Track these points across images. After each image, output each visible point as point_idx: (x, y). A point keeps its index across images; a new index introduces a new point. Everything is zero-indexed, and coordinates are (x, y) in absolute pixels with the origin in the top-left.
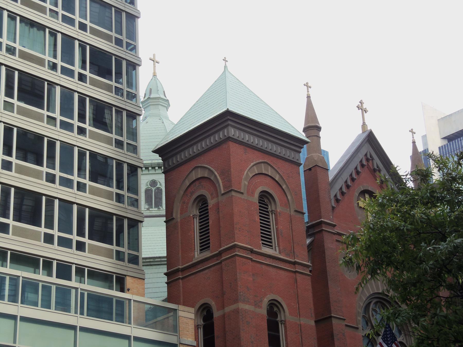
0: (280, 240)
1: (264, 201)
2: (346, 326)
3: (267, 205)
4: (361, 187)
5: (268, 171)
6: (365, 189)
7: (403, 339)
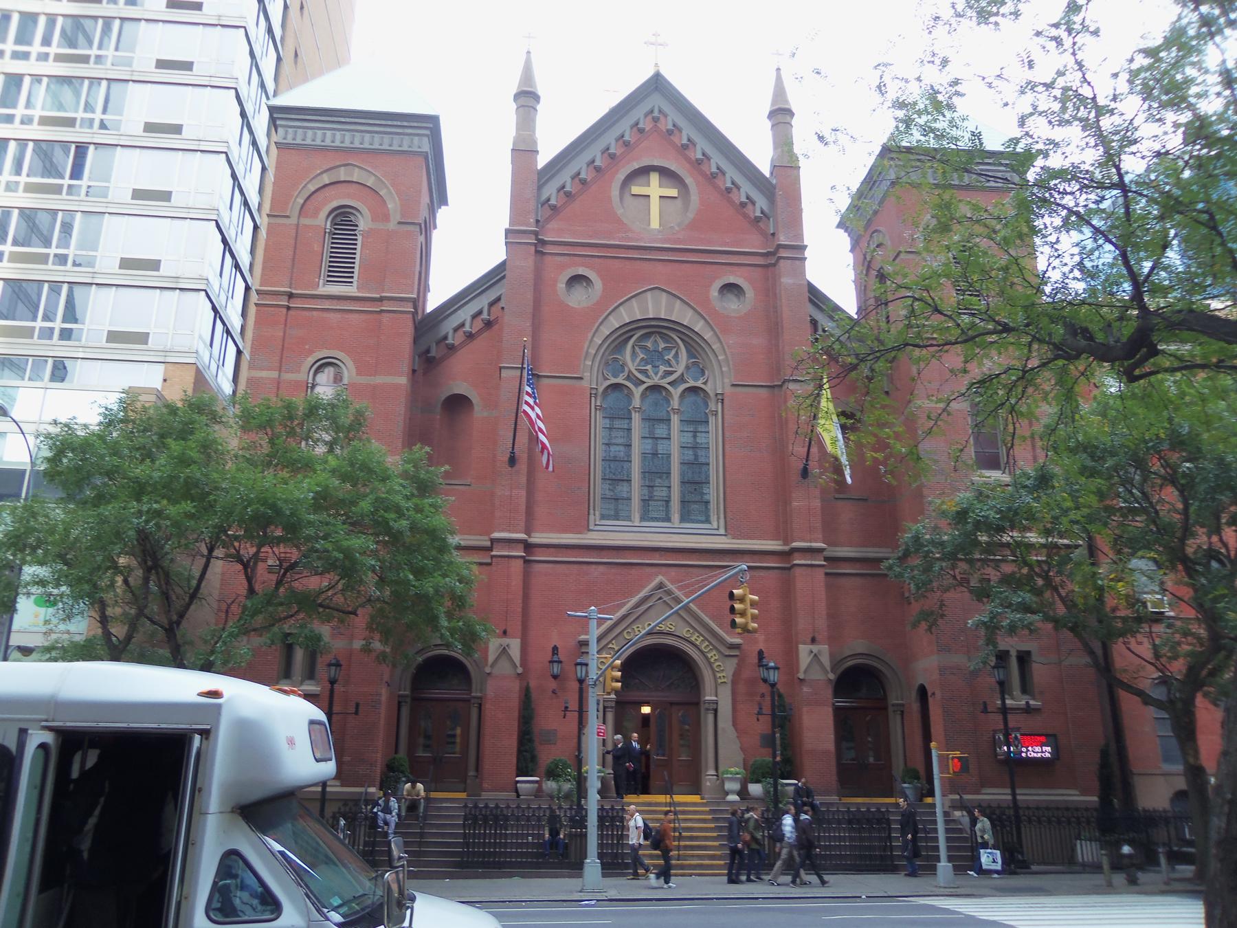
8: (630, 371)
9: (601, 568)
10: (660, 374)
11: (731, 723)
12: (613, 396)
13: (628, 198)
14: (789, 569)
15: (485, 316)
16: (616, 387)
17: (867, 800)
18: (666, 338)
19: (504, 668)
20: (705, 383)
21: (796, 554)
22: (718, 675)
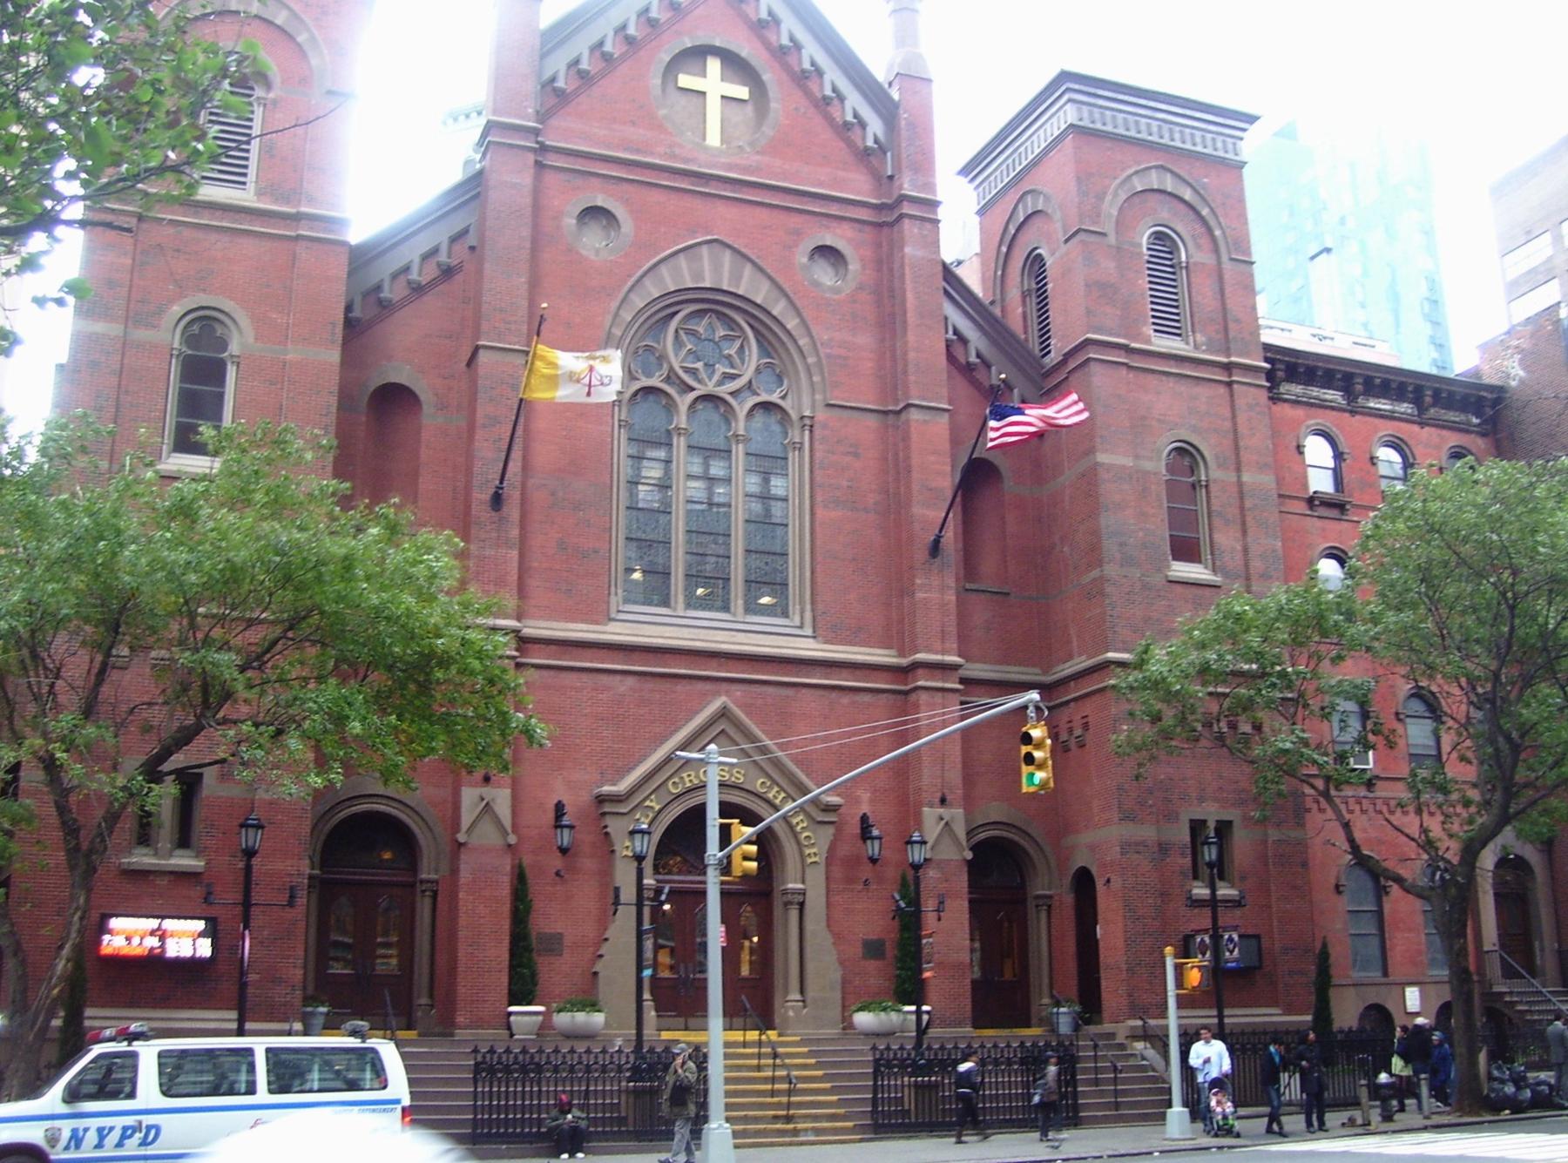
8: (671, 369)
9: (630, 681)
10: (716, 377)
11: (824, 924)
12: (649, 405)
13: (671, 89)
14: (906, 693)
15: (443, 257)
16: (649, 391)
17: (1005, 1032)
18: (730, 323)
19: (487, 836)
20: (783, 398)
21: (920, 672)
22: (807, 851)
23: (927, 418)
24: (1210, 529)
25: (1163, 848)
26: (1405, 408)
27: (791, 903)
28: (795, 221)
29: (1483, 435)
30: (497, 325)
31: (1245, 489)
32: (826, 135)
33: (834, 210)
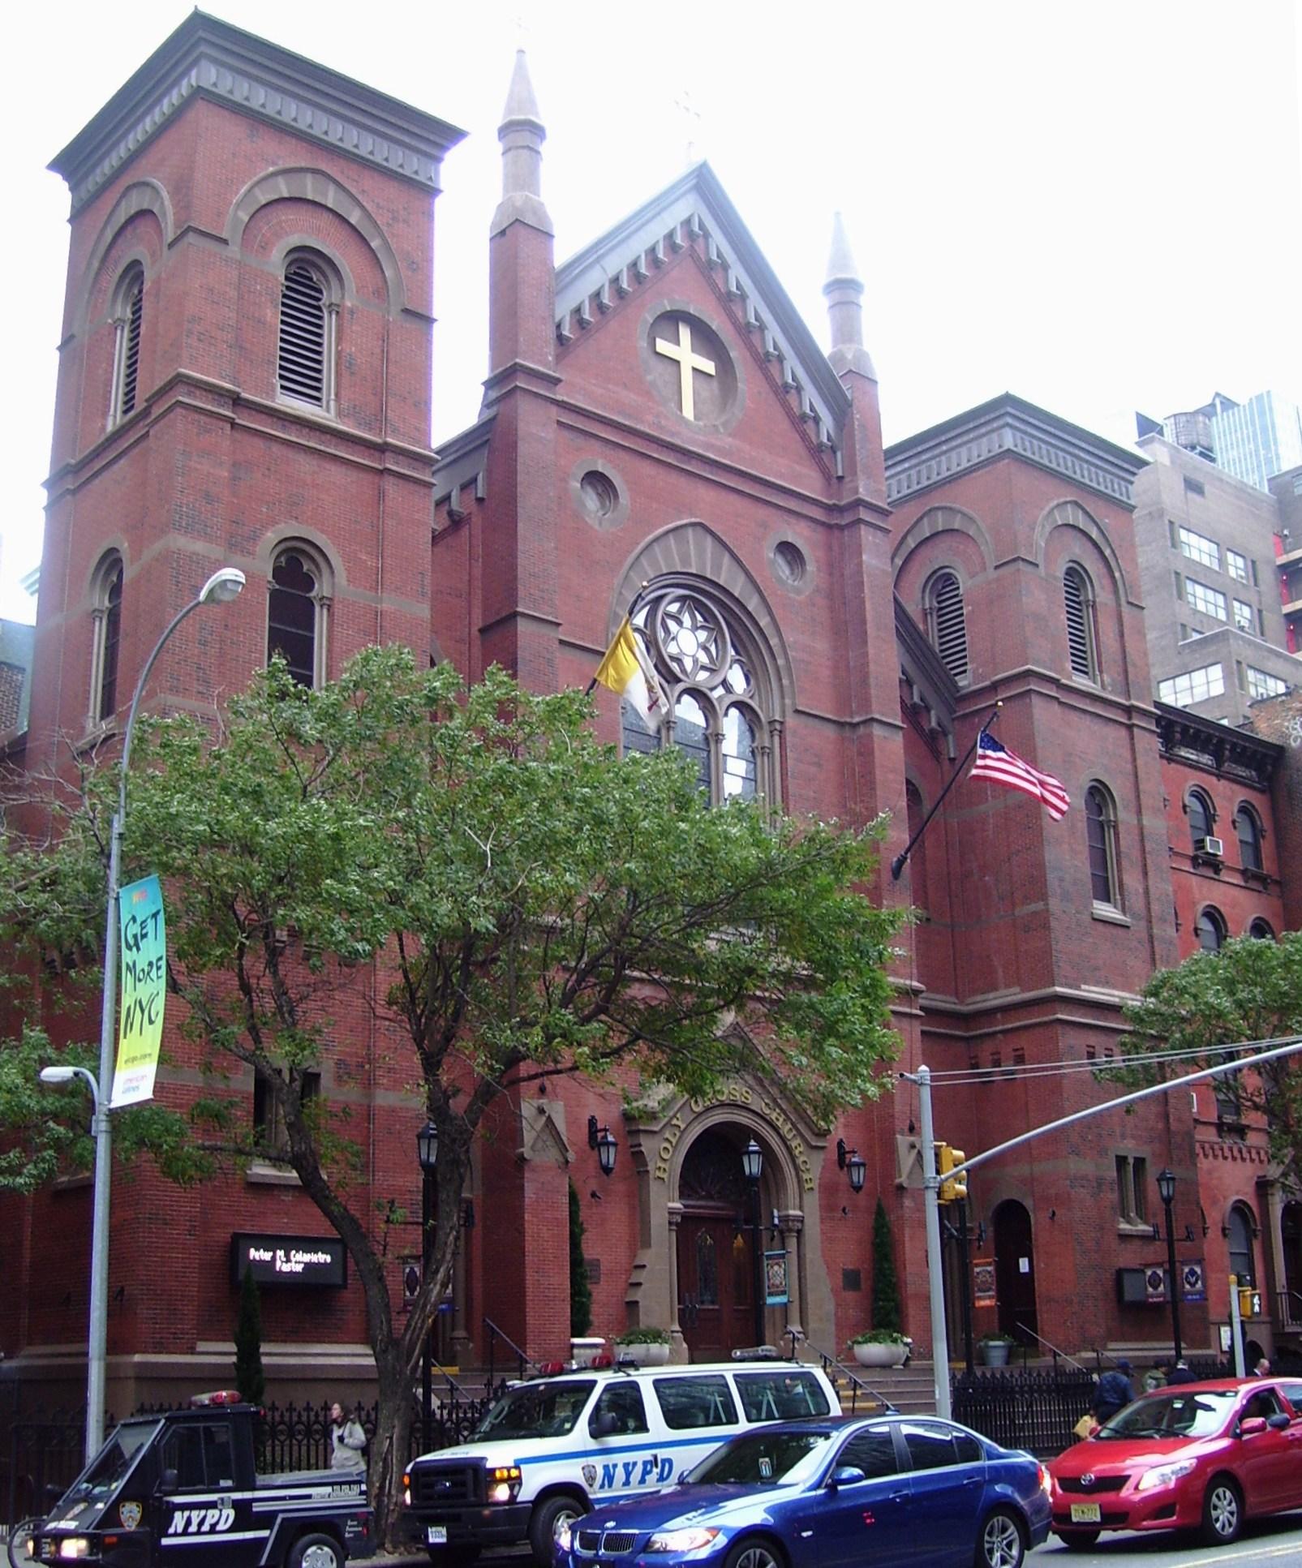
0: (345, 381)
1: (311, 279)
2: (561, 642)
3: (321, 292)
4: (666, 302)
5: (325, 195)
6: (674, 308)
7: (751, 698)
23: (886, 735)
24: (1119, 871)
25: (1100, 1182)
26: (1206, 759)
27: (790, 1230)
28: (762, 512)
29: (1262, 791)
30: (532, 591)
31: (1146, 832)
32: (784, 425)
33: (793, 504)
